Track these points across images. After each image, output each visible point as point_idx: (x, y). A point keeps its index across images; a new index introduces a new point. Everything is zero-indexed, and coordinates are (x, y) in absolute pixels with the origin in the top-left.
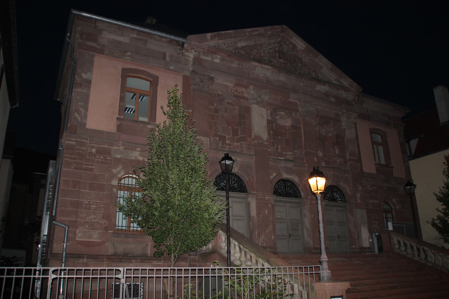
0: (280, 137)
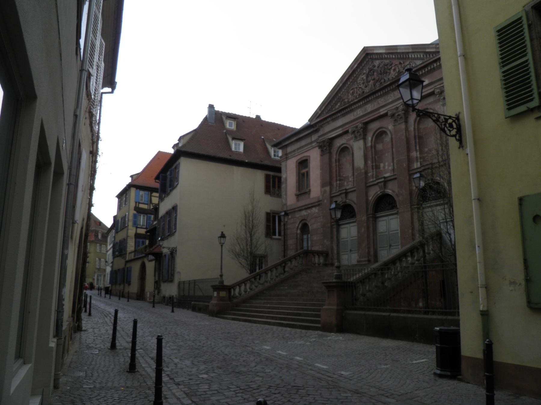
0: (387, 155)
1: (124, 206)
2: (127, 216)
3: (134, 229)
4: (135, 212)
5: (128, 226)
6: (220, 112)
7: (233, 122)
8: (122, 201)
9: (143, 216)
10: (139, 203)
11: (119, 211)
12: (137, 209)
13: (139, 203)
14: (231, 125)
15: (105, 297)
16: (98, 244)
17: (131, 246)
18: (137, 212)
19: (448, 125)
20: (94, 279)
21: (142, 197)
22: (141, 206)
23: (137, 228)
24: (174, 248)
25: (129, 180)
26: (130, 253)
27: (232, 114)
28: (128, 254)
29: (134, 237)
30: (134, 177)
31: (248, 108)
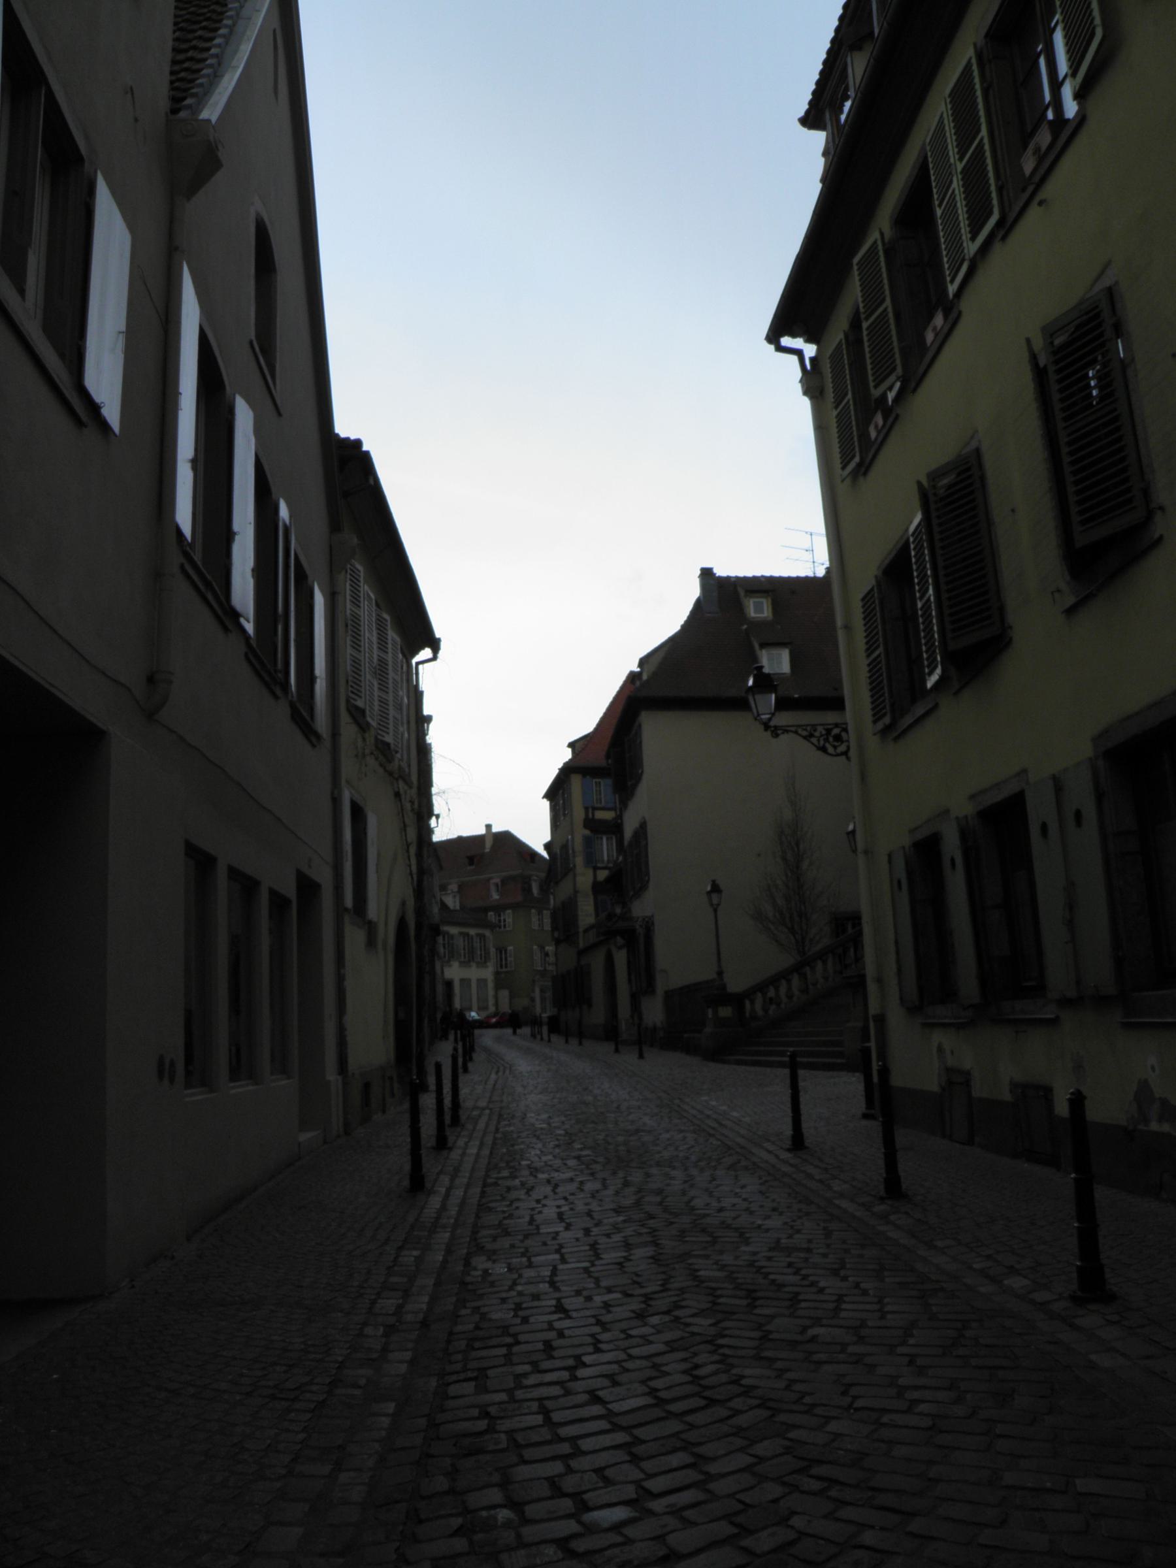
1: (562, 818)
2: (570, 843)
3: (590, 872)
4: (587, 832)
5: (575, 866)
6: (733, 579)
7: (764, 600)
8: (558, 808)
9: (607, 839)
10: (594, 809)
11: (556, 830)
12: (590, 823)
13: (594, 809)
14: (758, 610)
15: (549, 1041)
16: (533, 911)
17: (587, 913)
18: (592, 831)
19: (831, 739)
20: (533, 1000)
21: (600, 794)
22: (600, 815)
23: (595, 869)
24: (647, 917)
25: (567, 755)
26: (586, 931)
27: (763, 579)
28: (581, 935)
29: (590, 893)
30: (577, 745)
31: (807, 551)
